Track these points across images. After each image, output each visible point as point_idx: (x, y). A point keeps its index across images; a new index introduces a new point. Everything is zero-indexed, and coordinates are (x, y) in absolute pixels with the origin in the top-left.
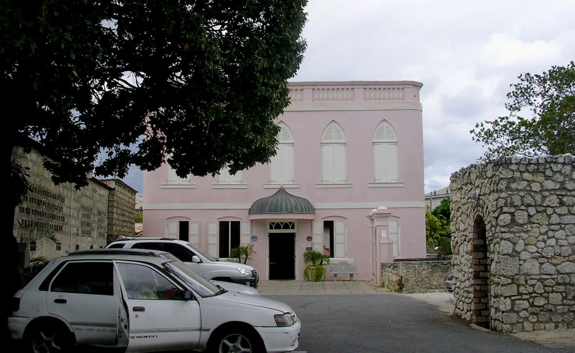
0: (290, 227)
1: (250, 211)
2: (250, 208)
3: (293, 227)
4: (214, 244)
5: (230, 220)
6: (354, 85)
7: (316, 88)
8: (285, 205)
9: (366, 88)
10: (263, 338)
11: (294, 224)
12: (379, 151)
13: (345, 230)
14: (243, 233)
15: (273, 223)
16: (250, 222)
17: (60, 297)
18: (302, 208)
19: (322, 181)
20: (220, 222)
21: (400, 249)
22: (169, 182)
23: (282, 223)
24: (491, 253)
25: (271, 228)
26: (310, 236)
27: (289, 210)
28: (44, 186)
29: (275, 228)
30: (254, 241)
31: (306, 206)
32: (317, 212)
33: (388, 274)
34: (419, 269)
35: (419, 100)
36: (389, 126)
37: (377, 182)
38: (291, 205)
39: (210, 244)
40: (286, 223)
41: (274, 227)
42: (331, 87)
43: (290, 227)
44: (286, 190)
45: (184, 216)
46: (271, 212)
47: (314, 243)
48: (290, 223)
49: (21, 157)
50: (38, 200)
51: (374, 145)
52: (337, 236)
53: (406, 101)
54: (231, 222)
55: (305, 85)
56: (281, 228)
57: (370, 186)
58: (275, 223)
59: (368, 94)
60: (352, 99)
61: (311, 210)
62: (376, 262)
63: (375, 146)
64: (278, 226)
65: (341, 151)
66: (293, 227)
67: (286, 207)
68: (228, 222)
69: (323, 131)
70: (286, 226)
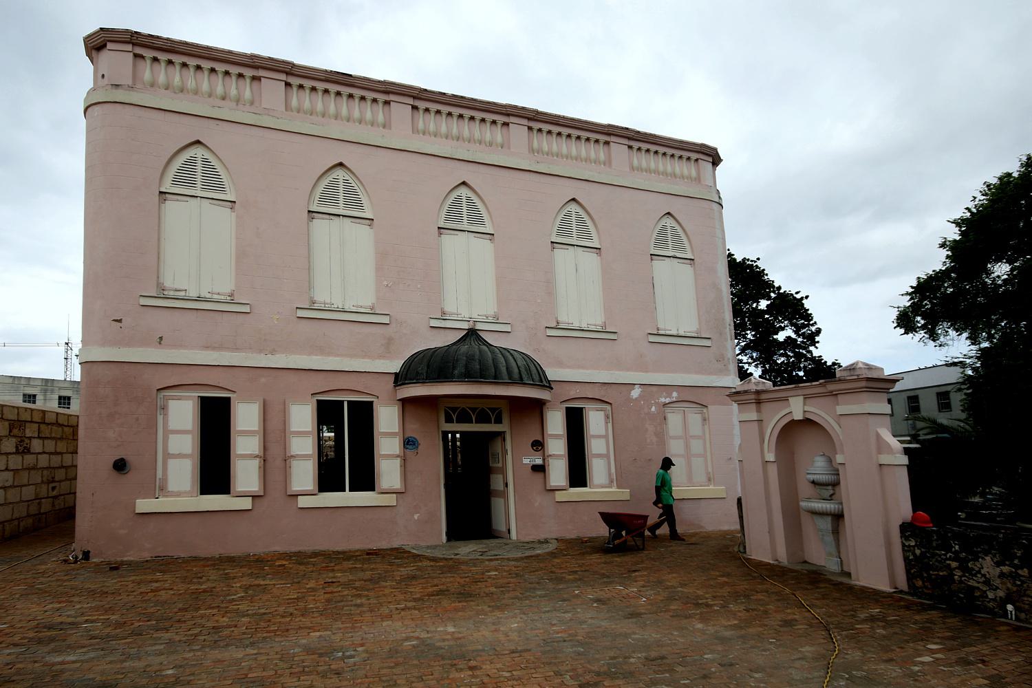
1: (400, 379)
5: (346, 398)
6: (508, 115)
8: (504, 364)
9: (142, 57)
11: (448, 408)
13: (704, 431)
16: (400, 403)
18: (520, 373)
20: (567, 408)
21: (613, 470)
22: (315, 305)
26: (540, 439)
27: (516, 376)
36: (677, 227)
37: (661, 332)
38: (518, 367)
39: (550, 456)
42: (565, 131)
44: (481, 334)
46: (469, 376)
52: (310, 429)
53: (512, 150)
55: (613, 135)
56: (490, 422)
57: (652, 339)
58: (476, 409)
59: (421, 119)
60: (608, 162)
61: (544, 383)
67: (507, 368)
69: (315, 185)
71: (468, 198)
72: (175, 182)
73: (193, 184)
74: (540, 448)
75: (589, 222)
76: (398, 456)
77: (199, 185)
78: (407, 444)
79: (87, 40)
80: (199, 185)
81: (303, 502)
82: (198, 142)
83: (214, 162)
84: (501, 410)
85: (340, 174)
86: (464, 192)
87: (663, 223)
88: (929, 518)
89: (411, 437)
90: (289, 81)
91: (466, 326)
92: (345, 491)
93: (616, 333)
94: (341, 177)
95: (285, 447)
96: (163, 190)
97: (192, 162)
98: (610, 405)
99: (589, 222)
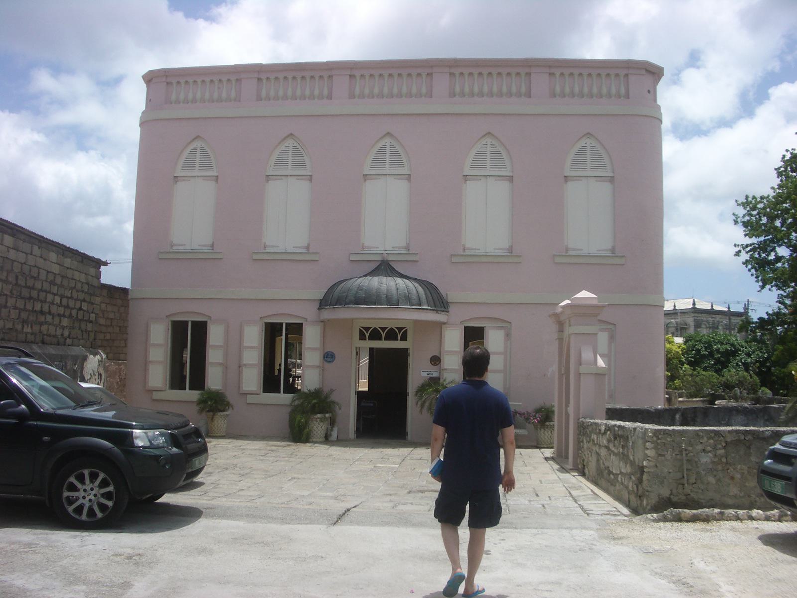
0: (383, 336)
2: (322, 299)
3: (404, 338)
4: (494, 371)
5: (285, 321)
7: (457, 71)
9: (554, 74)
11: (362, 327)
12: (575, 193)
14: (307, 346)
15: (367, 329)
19: (464, 250)
20: (466, 328)
23: (383, 329)
24: (110, 340)
25: (362, 337)
26: (438, 355)
29: (370, 339)
30: (330, 362)
31: (430, 295)
32: (452, 309)
33: (596, 448)
34: (690, 448)
35: (655, 100)
37: (571, 253)
39: (245, 365)
40: (375, 328)
41: (367, 336)
44: (393, 265)
45: (191, 313)
47: (151, 362)
48: (400, 329)
51: (566, 181)
54: (287, 324)
64: (375, 335)
65: (499, 192)
66: (404, 338)
70: (391, 335)
71: (392, 146)
72: (185, 167)
73: (193, 168)
74: (438, 363)
75: (504, 153)
76: (318, 367)
77: (488, 167)
78: (327, 357)
79: (144, 77)
80: (488, 167)
81: (250, 399)
82: (198, 137)
83: (400, 150)
84: (407, 330)
85: (290, 142)
86: (387, 141)
87: (582, 142)
88: (772, 461)
89: (329, 352)
90: (168, 81)
91: (379, 258)
92: (185, 389)
93: (624, 256)
94: (588, 144)
95: (146, 352)
96: (267, 174)
97: (193, 152)
98: (509, 324)
99: (504, 153)
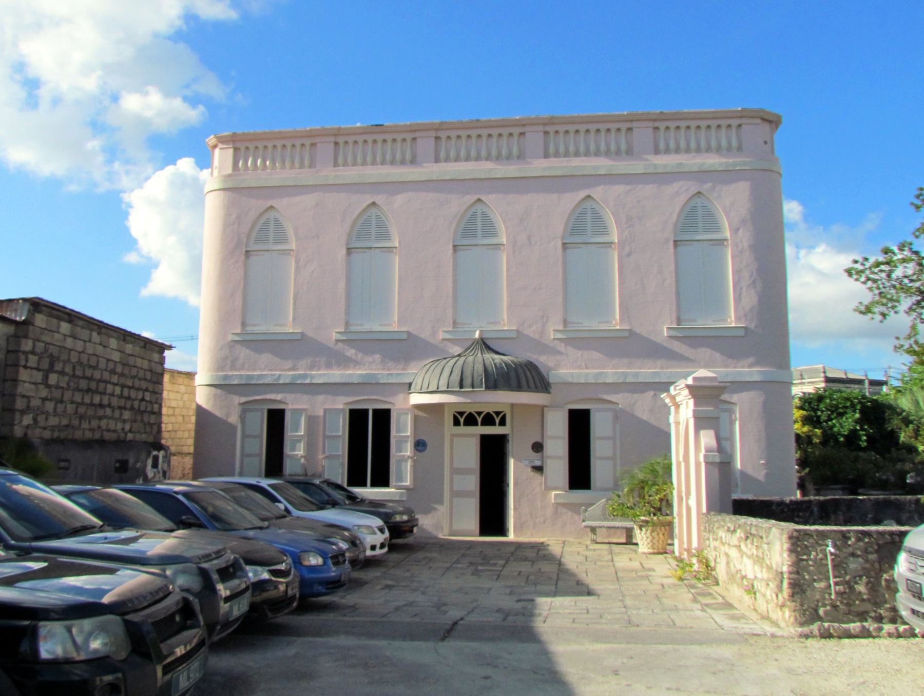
0: (497, 421)
3: (503, 423)
5: (371, 407)
10: (155, 340)
15: (461, 414)
17: (198, 203)
20: (508, 434)
23: (479, 413)
26: (540, 441)
28: (146, 94)
40: (470, 414)
43: (497, 421)
47: (549, 457)
48: (498, 413)
49: (272, 618)
50: (67, 469)
54: (375, 411)
62: (689, 509)
63: (567, 250)
66: (503, 423)
68: (366, 411)
